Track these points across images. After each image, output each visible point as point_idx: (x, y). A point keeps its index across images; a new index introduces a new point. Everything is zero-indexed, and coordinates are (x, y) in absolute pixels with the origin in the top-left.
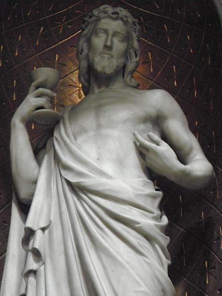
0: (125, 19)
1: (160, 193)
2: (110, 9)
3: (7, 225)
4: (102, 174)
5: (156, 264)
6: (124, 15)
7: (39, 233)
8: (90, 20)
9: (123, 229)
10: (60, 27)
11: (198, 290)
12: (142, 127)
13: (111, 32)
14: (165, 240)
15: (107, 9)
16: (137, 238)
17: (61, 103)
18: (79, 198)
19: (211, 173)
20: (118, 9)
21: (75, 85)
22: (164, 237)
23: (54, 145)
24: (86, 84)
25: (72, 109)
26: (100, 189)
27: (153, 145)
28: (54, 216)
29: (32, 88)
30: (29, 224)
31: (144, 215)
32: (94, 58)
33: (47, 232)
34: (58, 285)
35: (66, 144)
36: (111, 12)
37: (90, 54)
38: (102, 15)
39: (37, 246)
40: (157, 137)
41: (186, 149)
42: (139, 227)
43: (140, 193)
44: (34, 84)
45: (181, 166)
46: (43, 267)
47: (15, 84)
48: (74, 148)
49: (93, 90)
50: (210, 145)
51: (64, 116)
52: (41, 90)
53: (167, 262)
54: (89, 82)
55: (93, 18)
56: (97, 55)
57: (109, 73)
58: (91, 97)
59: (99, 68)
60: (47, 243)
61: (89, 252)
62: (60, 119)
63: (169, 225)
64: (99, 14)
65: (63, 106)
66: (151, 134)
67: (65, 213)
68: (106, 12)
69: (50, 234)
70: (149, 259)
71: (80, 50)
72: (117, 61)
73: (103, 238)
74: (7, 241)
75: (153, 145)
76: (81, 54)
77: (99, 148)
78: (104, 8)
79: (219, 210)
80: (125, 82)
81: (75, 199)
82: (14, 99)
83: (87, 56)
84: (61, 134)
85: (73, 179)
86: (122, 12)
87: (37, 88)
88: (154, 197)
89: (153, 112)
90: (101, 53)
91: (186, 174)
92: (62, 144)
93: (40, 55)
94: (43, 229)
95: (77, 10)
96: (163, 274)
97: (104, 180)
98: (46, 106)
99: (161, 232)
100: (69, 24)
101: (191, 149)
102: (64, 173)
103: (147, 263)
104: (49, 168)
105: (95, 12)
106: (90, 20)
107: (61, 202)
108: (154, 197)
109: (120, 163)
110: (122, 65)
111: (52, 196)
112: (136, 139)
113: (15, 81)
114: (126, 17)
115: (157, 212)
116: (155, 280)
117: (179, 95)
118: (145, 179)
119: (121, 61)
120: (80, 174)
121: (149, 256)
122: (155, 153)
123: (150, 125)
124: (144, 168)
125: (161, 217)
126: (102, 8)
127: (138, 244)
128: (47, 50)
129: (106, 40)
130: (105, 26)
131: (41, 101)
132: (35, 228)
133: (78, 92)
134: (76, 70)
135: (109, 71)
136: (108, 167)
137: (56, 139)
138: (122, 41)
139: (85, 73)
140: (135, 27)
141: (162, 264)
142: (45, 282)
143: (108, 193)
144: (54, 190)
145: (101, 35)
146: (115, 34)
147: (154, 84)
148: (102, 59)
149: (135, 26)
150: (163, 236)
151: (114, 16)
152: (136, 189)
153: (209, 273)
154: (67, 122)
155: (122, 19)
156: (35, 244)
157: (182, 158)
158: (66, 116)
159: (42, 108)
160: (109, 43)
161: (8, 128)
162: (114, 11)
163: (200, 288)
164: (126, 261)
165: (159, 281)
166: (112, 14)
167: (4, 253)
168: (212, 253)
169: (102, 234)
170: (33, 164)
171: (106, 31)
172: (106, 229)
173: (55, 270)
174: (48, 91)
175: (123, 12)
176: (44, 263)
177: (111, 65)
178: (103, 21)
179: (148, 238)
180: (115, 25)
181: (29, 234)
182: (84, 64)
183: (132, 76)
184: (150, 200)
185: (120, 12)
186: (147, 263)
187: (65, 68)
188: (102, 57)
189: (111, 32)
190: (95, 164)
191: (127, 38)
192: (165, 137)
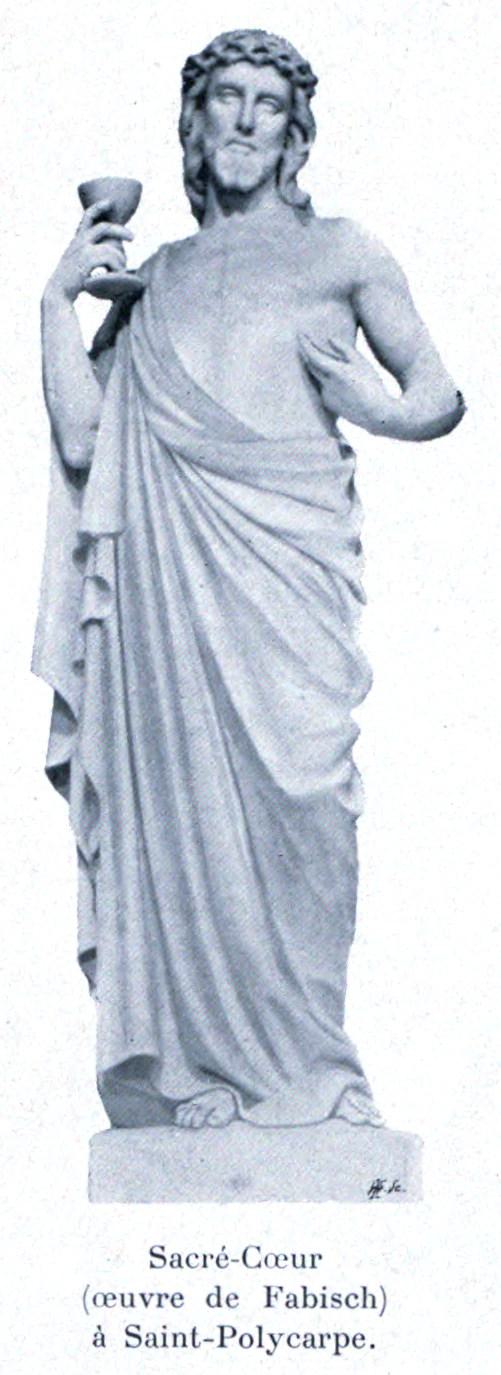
13: (251, 96)
37: (209, 143)
59: (226, 177)
129: (241, 114)
135: (247, 181)
146: (260, 98)
151: (259, 57)
160: (246, 121)
171: (240, 92)
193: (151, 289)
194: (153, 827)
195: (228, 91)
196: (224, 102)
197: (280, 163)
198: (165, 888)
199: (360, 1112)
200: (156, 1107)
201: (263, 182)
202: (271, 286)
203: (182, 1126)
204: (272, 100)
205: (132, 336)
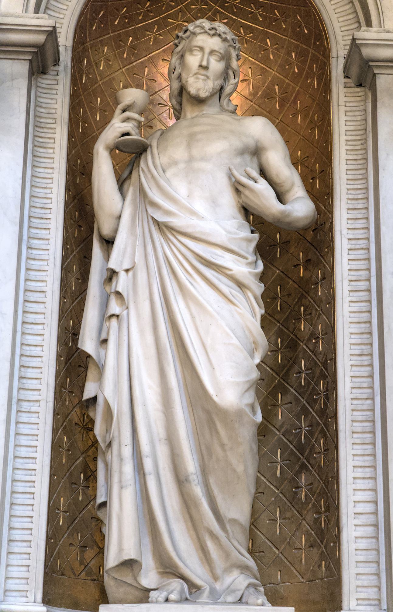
0: (224, 36)
1: (256, 236)
2: (207, 24)
3: (88, 260)
4: (193, 213)
5: (249, 316)
6: (223, 31)
7: (122, 275)
8: (184, 36)
9: (214, 276)
10: (151, 38)
11: (292, 338)
12: (238, 160)
13: (207, 51)
14: (259, 288)
15: (204, 24)
16: (228, 286)
17: (148, 124)
18: (167, 240)
19: (313, 213)
20: (216, 24)
21: (165, 104)
22: (259, 285)
23: (139, 176)
24: (177, 107)
25: (161, 135)
26: (189, 230)
27: (250, 183)
28: (139, 259)
29: (118, 111)
30: (112, 264)
31: (238, 260)
32: (187, 78)
33: (131, 273)
34: (142, 332)
35: (153, 177)
36: (208, 28)
37: (184, 75)
38: (198, 30)
39: (120, 289)
40: (255, 174)
41: (287, 186)
42: (232, 274)
43: (234, 236)
44: (120, 107)
45: (280, 207)
46: (125, 312)
47: (99, 103)
48: (162, 183)
49: (185, 115)
50: (299, 27)
51: (152, 144)
52: (127, 114)
53: (260, 311)
54: (181, 104)
55: (188, 33)
56: (191, 75)
57: (204, 96)
58: (183, 123)
59: (192, 90)
60: (130, 286)
61: (176, 299)
62: (147, 148)
63: (263, 273)
64: (194, 30)
65: (151, 127)
66: (249, 170)
67: (151, 255)
68: (203, 28)
69: (134, 276)
70: (241, 310)
71: (173, 67)
72: (214, 84)
73: (192, 284)
74: (88, 278)
75: (250, 183)
76: (174, 72)
77: (190, 183)
78: (201, 23)
79: (319, 253)
80: (221, 106)
81: (162, 240)
82: (98, 119)
83: (179, 77)
84: (148, 165)
85: (161, 218)
86: (221, 28)
87: (124, 111)
88: (249, 241)
89: (251, 143)
90: (195, 74)
91: (285, 214)
92: (149, 177)
93: (128, 69)
94: (127, 271)
95: (170, 19)
96: (255, 325)
97: (194, 221)
98: (133, 132)
99: (256, 280)
100: (160, 35)
101: (293, 185)
102: (150, 210)
103: (240, 314)
104: (134, 200)
105: (191, 27)
106: (184, 36)
107: (146, 242)
108: (249, 241)
109: (214, 202)
110: (218, 86)
111: (137, 235)
112: (232, 174)
113: (99, 99)
114: (225, 33)
115: (252, 258)
116: (247, 332)
117: (281, 120)
118: (240, 219)
119: (218, 83)
120: (168, 213)
121: (242, 307)
122: (251, 190)
123: (247, 157)
124: (240, 208)
125: (256, 262)
126: (198, 22)
127: (229, 293)
128: (135, 63)
129: (202, 60)
130: (200, 44)
131: (128, 127)
132: (117, 270)
133: (168, 111)
134: (167, 86)
135: (203, 94)
136: (199, 206)
137: (143, 170)
138: (219, 61)
139: (176, 94)
140: (235, 45)
141: (254, 314)
142: (128, 328)
143: (198, 235)
144: (138, 230)
145: (195, 53)
146: (212, 52)
147: (254, 105)
148: (196, 81)
149: (235, 44)
150: (256, 284)
151: (212, 32)
152: (229, 232)
153: (306, 320)
154: (155, 150)
155: (219, 35)
156: (118, 286)
157: (281, 197)
158: (154, 144)
159: (128, 134)
160: (204, 63)
161: (89, 153)
162: (212, 26)
163: (294, 335)
164: (215, 311)
165: (251, 332)
166: (210, 29)
167: (84, 291)
168: (309, 298)
169: (190, 280)
170: (117, 196)
171: (202, 49)
172: (195, 276)
173: (139, 316)
174: (136, 116)
175: (222, 28)
176: (127, 308)
177: (207, 87)
178: (200, 37)
179: (241, 285)
180: (214, 43)
181: (112, 275)
182: (176, 85)
183: (229, 99)
184: (244, 244)
185: (217, 28)
186: (240, 314)
187: (154, 84)
188: (197, 78)
189: (207, 51)
190: (185, 202)
191: (225, 58)
192: (263, 173)
193: (151, 148)
194: (140, 217)
195: (197, 48)
196: (193, 55)
197: (222, 88)
198: (353, 95)
199: (64, 342)
200: (138, 593)
201: (212, 95)
202: (240, 47)
203: (157, 602)
204: (218, 54)
205: (140, 169)
